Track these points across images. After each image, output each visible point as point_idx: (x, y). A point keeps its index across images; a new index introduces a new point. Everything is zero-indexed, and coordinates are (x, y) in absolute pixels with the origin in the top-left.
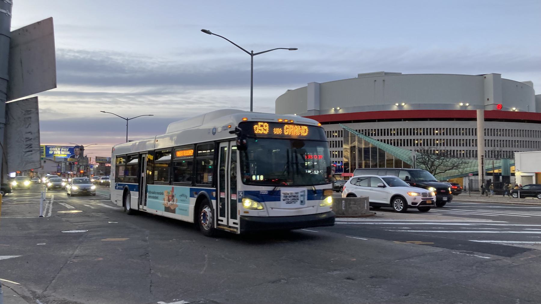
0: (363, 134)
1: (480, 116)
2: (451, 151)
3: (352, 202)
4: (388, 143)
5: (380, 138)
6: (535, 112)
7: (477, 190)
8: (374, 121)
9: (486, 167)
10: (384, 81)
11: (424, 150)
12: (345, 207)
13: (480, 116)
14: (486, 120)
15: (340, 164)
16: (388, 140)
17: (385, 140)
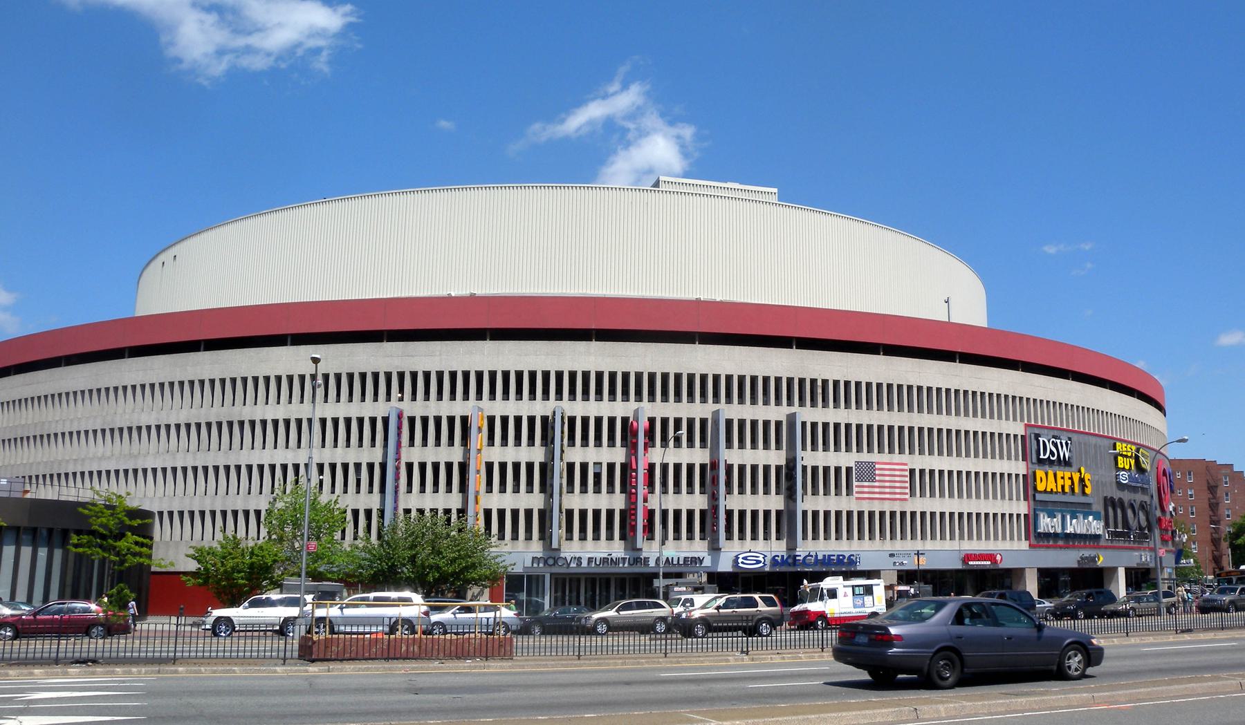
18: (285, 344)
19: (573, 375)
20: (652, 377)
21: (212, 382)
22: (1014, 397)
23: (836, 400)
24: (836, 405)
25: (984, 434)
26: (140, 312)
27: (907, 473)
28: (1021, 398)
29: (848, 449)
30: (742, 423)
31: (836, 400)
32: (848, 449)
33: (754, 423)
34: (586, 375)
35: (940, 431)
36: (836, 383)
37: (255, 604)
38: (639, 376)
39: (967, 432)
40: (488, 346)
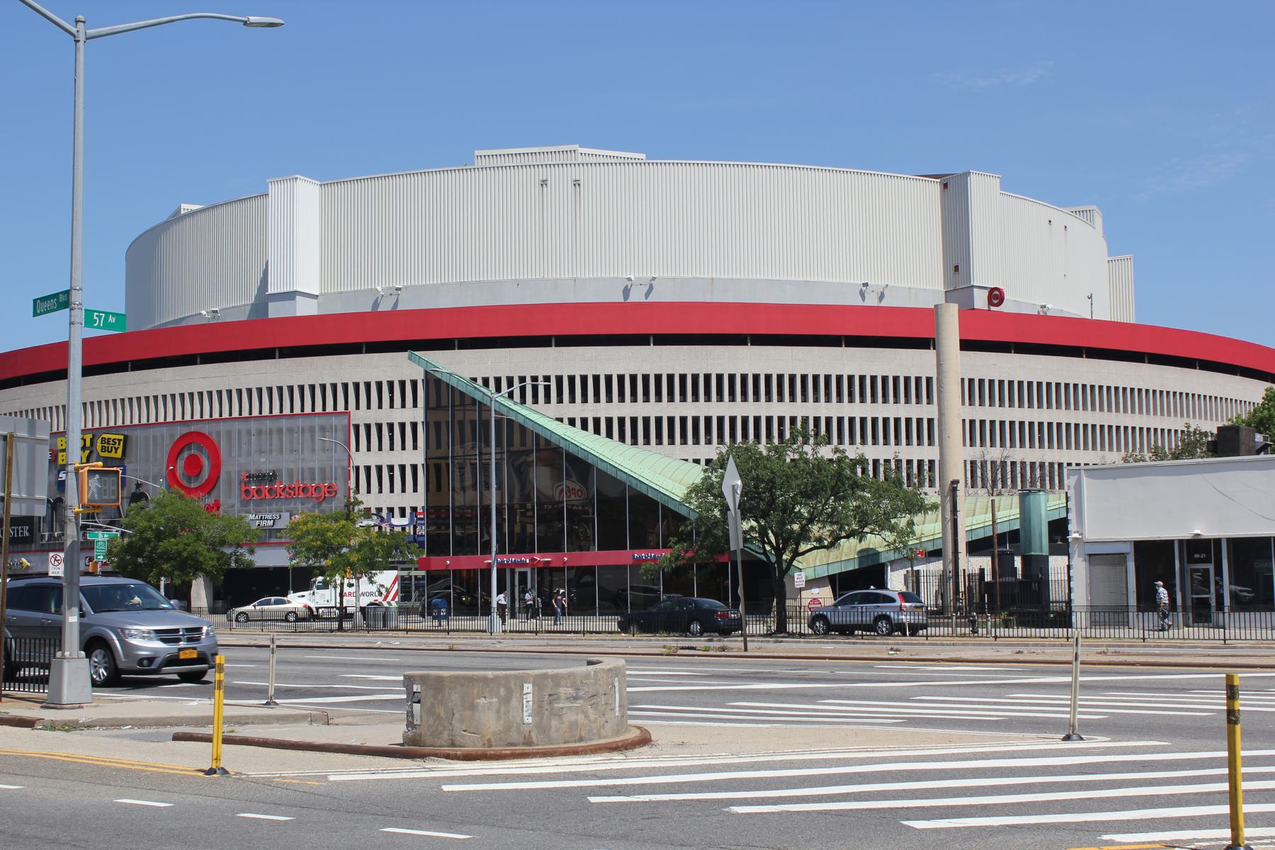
0: (511, 395)
1: (951, 333)
2: (984, 463)
3: (565, 691)
4: (597, 431)
5: (568, 410)
6: (1133, 321)
7: (84, 535)
8: (641, 340)
9: (965, 523)
10: (577, 183)
11: (898, 462)
12: (538, 710)
13: (951, 333)
14: (966, 345)
15: (405, 521)
16: (609, 421)
17: (597, 421)
18: (360, 352)
19: (633, 378)
20: (658, 378)
21: (156, 398)
22: (1161, 392)
23: (839, 394)
24: (896, 401)
25: (1169, 431)
26: (157, 323)
27: (61, 429)
28: (1168, 393)
29: (886, 442)
30: (708, 420)
31: (839, 394)
32: (886, 442)
33: (769, 420)
34: (609, 379)
35: (1102, 427)
36: (1020, 383)
37: (396, 594)
38: (671, 378)
39: (1156, 430)
40: (552, 352)
